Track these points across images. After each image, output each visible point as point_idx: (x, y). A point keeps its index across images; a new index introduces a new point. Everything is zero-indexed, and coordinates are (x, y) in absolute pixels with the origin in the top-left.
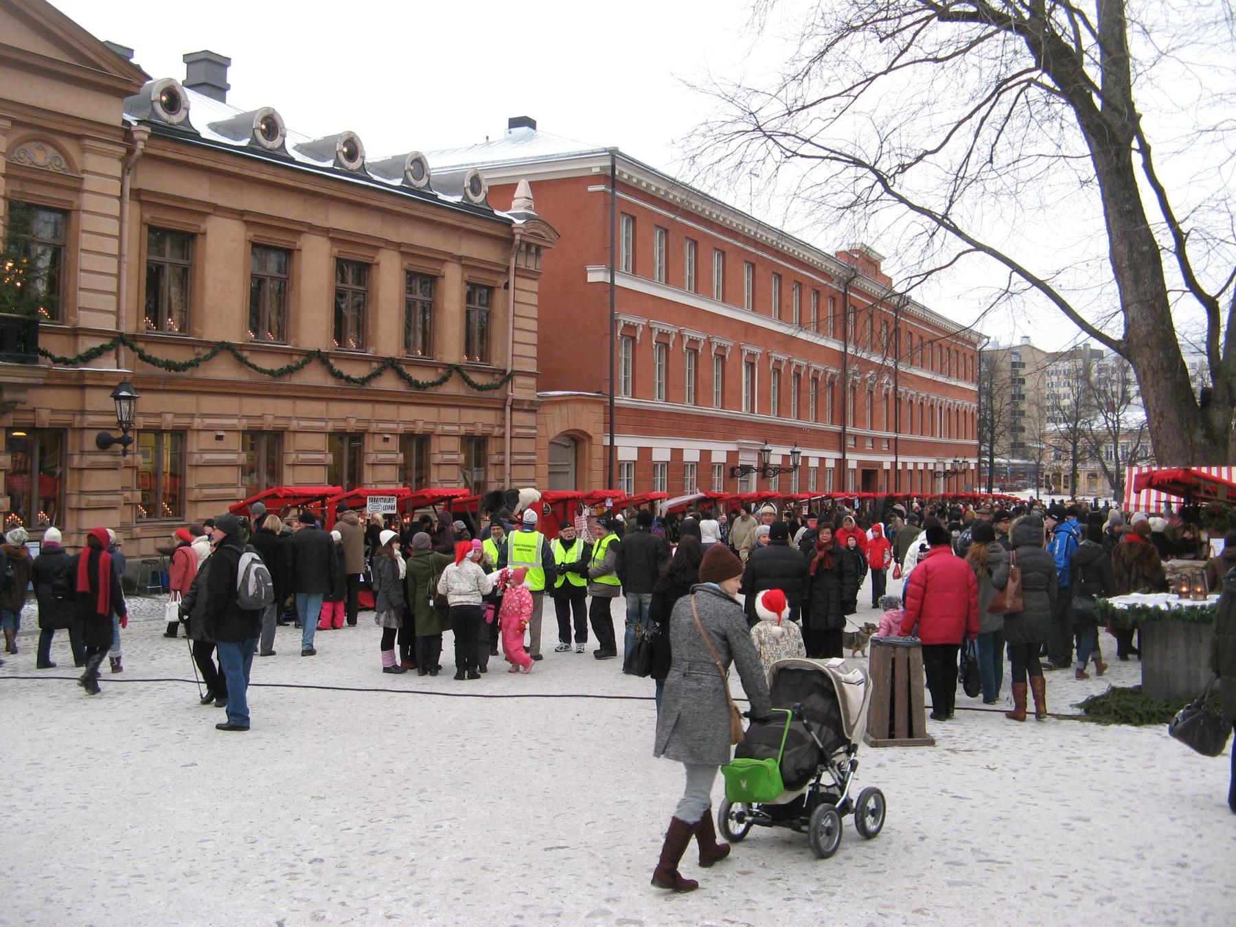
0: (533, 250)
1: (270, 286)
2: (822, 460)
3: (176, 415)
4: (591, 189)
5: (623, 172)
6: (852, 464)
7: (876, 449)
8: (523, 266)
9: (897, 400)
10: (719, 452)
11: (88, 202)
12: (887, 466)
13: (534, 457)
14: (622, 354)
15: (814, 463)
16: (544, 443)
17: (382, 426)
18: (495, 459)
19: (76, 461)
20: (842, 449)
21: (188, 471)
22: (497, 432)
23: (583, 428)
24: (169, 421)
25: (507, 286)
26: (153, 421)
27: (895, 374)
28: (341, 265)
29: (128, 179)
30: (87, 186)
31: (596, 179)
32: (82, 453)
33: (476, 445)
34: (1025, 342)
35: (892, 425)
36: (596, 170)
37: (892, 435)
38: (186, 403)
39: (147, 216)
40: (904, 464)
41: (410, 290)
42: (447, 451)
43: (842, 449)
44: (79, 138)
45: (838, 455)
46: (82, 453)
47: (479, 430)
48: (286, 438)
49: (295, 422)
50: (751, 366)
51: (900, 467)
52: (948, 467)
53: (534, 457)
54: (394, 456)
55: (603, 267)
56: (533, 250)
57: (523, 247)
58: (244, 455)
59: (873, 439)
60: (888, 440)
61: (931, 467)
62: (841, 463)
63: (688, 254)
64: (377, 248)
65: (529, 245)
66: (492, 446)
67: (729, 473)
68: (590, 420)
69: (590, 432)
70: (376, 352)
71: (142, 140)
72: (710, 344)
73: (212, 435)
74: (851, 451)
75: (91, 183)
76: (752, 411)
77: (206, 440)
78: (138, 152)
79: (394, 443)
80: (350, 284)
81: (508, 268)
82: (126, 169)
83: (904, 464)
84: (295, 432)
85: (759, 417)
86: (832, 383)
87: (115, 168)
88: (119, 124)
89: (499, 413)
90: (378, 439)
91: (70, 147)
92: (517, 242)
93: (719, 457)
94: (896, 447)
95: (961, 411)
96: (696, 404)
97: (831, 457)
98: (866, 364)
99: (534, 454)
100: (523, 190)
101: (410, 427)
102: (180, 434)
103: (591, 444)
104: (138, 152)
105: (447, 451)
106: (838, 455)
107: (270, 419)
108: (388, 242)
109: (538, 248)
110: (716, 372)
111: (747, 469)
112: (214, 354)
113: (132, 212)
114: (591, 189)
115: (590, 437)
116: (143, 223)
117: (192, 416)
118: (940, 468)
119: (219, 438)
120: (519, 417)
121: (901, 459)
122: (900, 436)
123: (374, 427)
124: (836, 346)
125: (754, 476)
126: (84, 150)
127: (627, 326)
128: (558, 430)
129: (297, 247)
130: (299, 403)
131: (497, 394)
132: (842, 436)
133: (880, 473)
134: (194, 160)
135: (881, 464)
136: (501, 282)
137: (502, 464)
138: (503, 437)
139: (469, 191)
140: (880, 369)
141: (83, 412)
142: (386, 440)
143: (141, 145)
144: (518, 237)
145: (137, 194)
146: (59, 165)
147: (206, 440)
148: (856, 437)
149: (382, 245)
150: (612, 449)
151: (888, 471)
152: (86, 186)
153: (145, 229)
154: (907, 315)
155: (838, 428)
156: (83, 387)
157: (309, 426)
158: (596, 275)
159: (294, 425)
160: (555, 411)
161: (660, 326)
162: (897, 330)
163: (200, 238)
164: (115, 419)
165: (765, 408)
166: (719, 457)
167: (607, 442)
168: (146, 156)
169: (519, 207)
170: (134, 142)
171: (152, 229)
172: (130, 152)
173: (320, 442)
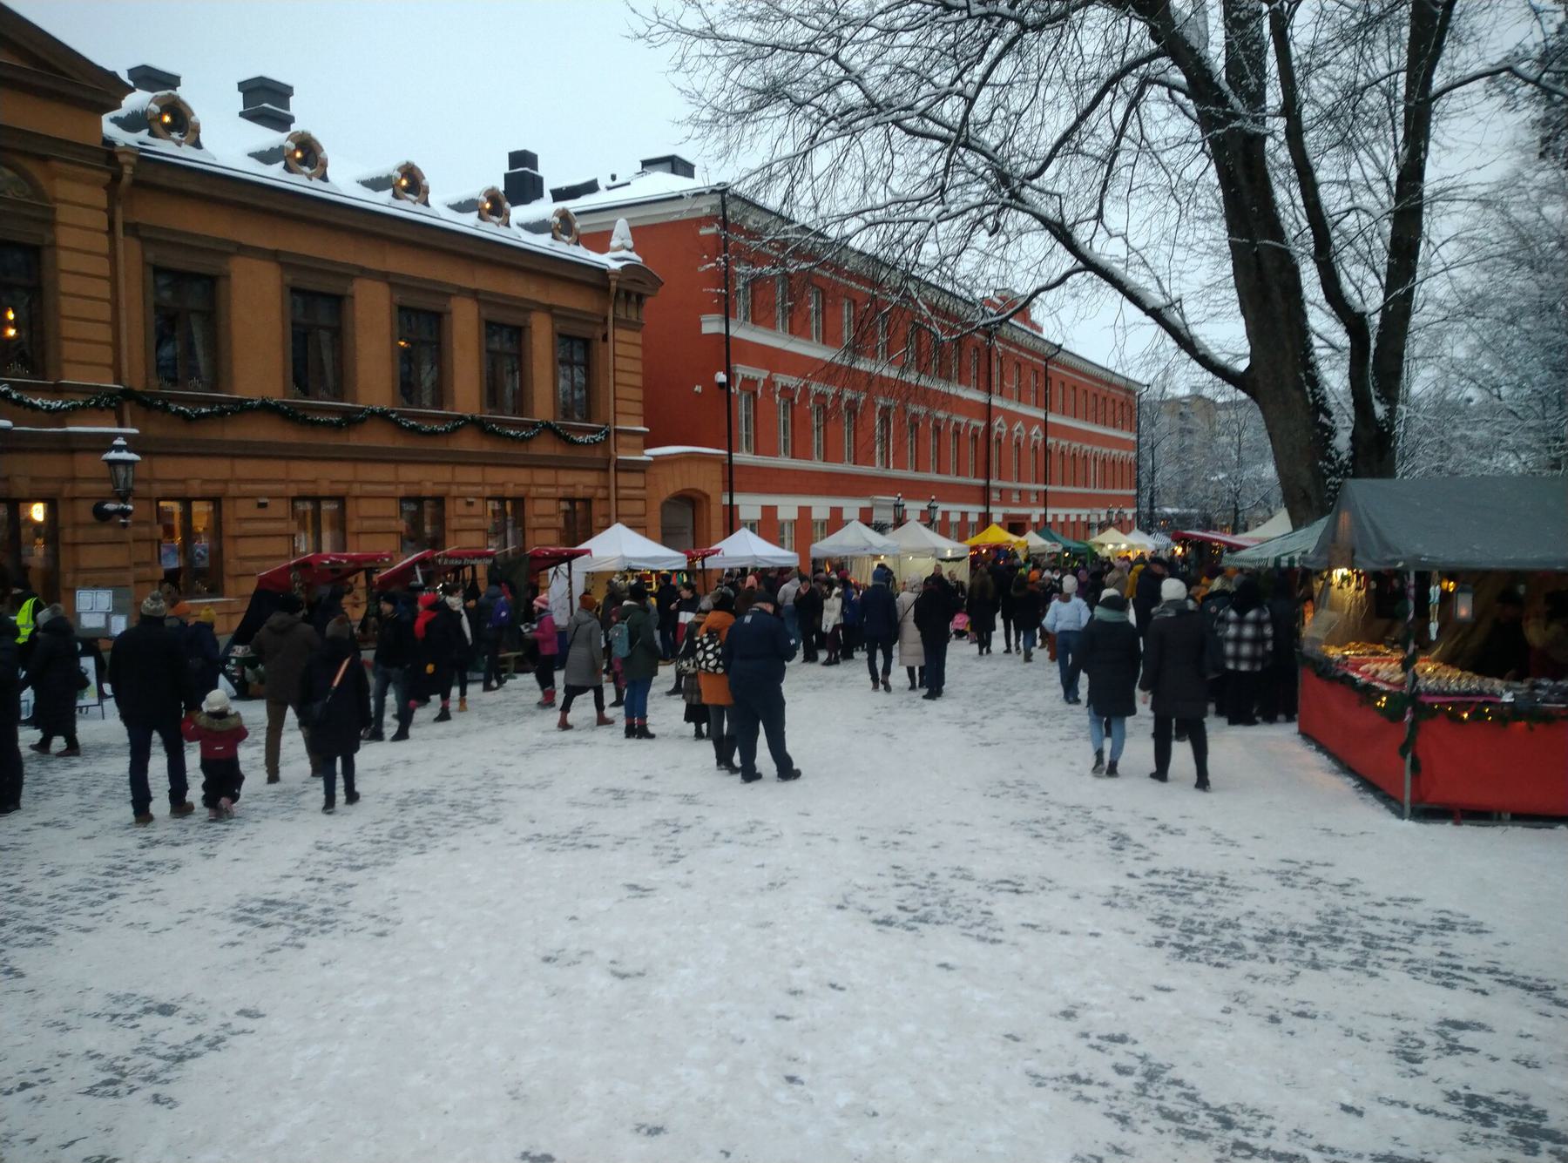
0: (634, 298)
3: (205, 481)
7: (1024, 501)
8: (623, 316)
9: (1047, 451)
11: (65, 237)
16: (657, 506)
17: (463, 489)
20: (987, 502)
22: (601, 493)
23: (700, 487)
24: (510, 491)
25: (605, 338)
26: (499, 491)
27: (1045, 425)
29: (119, 211)
30: (61, 218)
31: (708, 220)
32: (76, 525)
36: (707, 211)
37: (1041, 487)
38: (443, 473)
39: (150, 256)
40: (1055, 516)
43: (987, 502)
44: (43, 159)
45: (982, 509)
46: (76, 525)
47: (581, 492)
50: (885, 420)
51: (1049, 519)
52: (1103, 518)
54: (393, 523)
55: (717, 316)
56: (634, 298)
57: (622, 295)
59: (1020, 492)
60: (1037, 493)
61: (1084, 518)
64: (529, 311)
65: (628, 294)
69: (707, 490)
71: (128, 163)
72: (841, 397)
73: (251, 504)
74: (996, 504)
75: (64, 214)
77: (460, 503)
81: (606, 319)
82: (112, 186)
83: (1055, 516)
84: (235, 498)
86: (975, 436)
87: (101, 199)
88: (98, 144)
90: (460, 503)
91: (31, 166)
92: (613, 290)
94: (1045, 499)
98: (1011, 417)
100: (621, 231)
101: (570, 490)
102: (439, 501)
103: (709, 505)
104: (126, 180)
106: (982, 509)
109: (640, 297)
110: (932, 442)
112: (455, 429)
113: (130, 253)
115: (707, 497)
116: (145, 264)
118: (1094, 519)
119: (263, 506)
120: (623, 479)
121: (1051, 511)
122: (1050, 488)
123: (454, 490)
124: (980, 397)
127: (746, 380)
128: (671, 492)
131: (599, 454)
132: (986, 490)
135: (1028, 517)
136: (599, 333)
138: (607, 499)
140: (1029, 421)
142: (470, 504)
144: (613, 284)
145: (132, 229)
148: (1001, 491)
154: (1059, 364)
155: (982, 482)
156: (73, 451)
157: (471, 492)
158: (711, 325)
159: (357, 489)
161: (782, 380)
162: (1048, 379)
164: (110, 486)
165: (900, 465)
167: (726, 500)
170: (120, 166)
172: (116, 178)
173: (391, 507)
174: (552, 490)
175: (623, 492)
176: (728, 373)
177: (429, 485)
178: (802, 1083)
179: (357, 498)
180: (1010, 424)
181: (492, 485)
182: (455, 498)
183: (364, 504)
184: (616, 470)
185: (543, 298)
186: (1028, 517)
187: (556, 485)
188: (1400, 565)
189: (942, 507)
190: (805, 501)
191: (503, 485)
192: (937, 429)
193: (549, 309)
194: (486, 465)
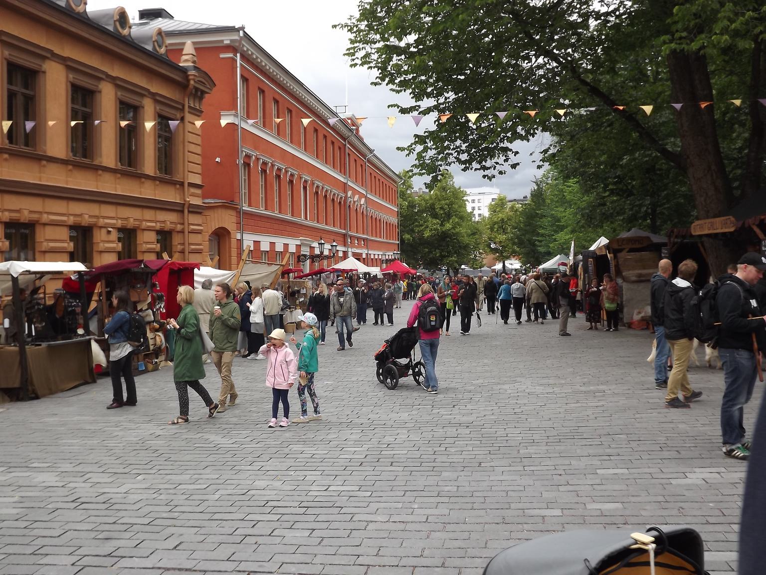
3: (31, 212)
4: (222, 56)
7: (359, 246)
8: (192, 105)
10: (293, 244)
13: (201, 247)
14: (242, 175)
22: (179, 227)
33: (165, 236)
35: (343, 226)
36: (227, 42)
47: (168, 226)
48: (173, 236)
49: (45, 216)
50: (305, 188)
52: (317, 252)
53: (201, 247)
54: (65, 245)
58: (120, 244)
64: (100, 79)
66: (176, 240)
67: (296, 260)
68: (227, 220)
70: (101, 163)
72: (301, 178)
76: (306, 218)
79: (114, 235)
81: (183, 106)
89: (179, 214)
90: (104, 231)
93: (292, 249)
95: (378, 218)
96: (280, 212)
98: (355, 192)
99: (200, 244)
101: (78, 219)
103: (230, 238)
107: (26, 213)
109: (203, 93)
114: (222, 56)
115: (228, 233)
118: (305, 251)
123: (102, 222)
129: (43, 70)
130: (158, 212)
138: (182, 232)
142: (109, 232)
144: (192, 82)
149: (104, 77)
150: (240, 242)
151: (364, 259)
159: (45, 218)
163: (41, 74)
169: (186, 61)
173: (64, 233)
174: (154, 224)
175: (192, 227)
177: (26, 213)
178: (506, 323)
179: (45, 224)
180: (360, 198)
181: (75, 215)
182: (101, 227)
183: (48, 229)
184: (189, 212)
185: (154, 89)
187: (156, 222)
188: (762, 185)
190: (273, 240)
191: (18, 211)
192: (264, 171)
193: (113, 80)
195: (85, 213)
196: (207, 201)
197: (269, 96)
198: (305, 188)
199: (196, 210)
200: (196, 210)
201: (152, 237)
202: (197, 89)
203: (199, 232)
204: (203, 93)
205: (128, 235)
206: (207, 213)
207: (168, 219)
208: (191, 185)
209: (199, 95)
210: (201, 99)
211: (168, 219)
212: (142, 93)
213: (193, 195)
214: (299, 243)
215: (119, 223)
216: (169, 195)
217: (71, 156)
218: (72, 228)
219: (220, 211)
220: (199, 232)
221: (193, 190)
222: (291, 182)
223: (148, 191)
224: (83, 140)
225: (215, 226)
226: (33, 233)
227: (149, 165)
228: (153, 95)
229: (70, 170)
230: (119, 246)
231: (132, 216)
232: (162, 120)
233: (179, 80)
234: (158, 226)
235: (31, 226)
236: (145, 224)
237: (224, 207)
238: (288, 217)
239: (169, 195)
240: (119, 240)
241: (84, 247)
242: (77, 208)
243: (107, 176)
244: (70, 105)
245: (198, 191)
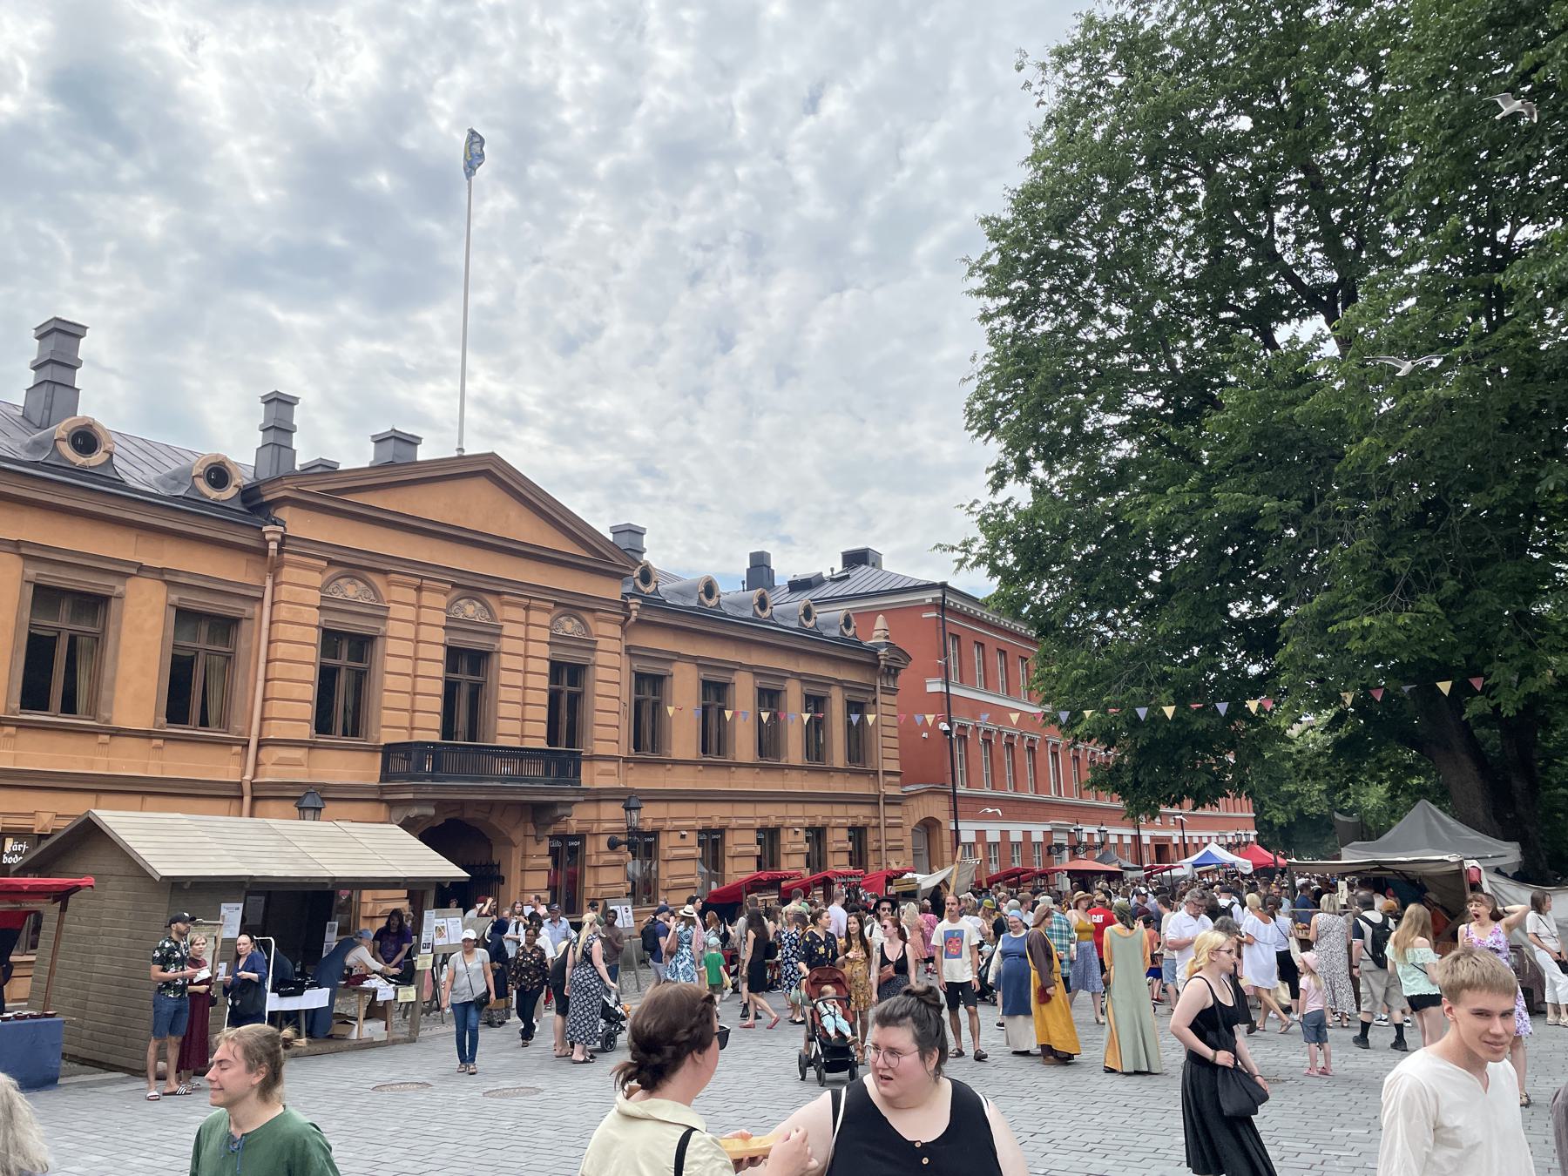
1: (343, 680)
2: (1120, 836)
5: (951, 600)
6: (1146, 840)
10: (1038, 832)
12: (1176, 840)
15: (1113, 840)
18: (875, 845)
19: (593, 861)
21: (783, 858)
22: (874, 822)
25: (875, 701)
28: (706, 685)
32: (598, 853)
34: (624, 542)
41: (638, 690)
42: (838, 839)
46: (598, 853)
47: (861, 822)
50: (1055, 754)
62: (1137, 839)
63: (999, 662)
66: (871, 836)
68: (937, 808)
73: (677, 835)
74: (1146, 828)
78: (633, 619)
79: (802, 835)
80: (343, 661)
85: (1065, 799)
90: (791, 832)
91: (376, 579)
93: (1038, 837)
97: (1128, 833)
101: (707, 822)
104: (633, 619)
105: (838, 839)
106: (1134, 832)
108: (141, 568)
109: (897, 669)
110: (1007, 759)
111: (1060, 847)
115: (939, 823)
117: (664, 819)
123: (788, 823)
125: (1066, 853)
126: (390, 584)
130: (701, 805)
133: (1171, 848)
134: (57, 500)
135: (1170, 839)
136: (870, 699)
137: (879, 850)
139: (638, 582)
141: (599, 821)
142: (683, 836)
143: (634, 614)
146: (366, 598)
147: (674, 839)
152: (391, 614)
153: (173, 612)
159: (734, 823)
160: (914, 802)
163: (245, 625)
164: (624, 825)
166: (1038, 837)
168: (640, 622)
171: (637, 674)
172: (627, 618)
173: (751, 837)
176: (950, 724)
186: (1170, 839)
187: (847, 817)
189: (1087, 829)
190: (1005, 827)
192: (987, 742)
193: (797, 676)
194: (599, 801)
195: (715, 814)
196: (908, 788)
197: (991, 648)
198: (1055, 754)
199: (893, 801)
200: (893, 801)
201: (843, 834)
202: (889, 667)
203: (899, 826)
204: (897, 669)
205: (769, 836)
206: (909, 802)
207: (861, 814)
208: (886, 773)
209: (892, 672)
210: (895, 676)
211: (861, 814)
212: (782, 676)
213: (890, 784)
214: (1048, 828)
215: (807, 823)
216: (861, 787)
217: (806, 763)
218: (850, 829)
219: (926, 799)
220: (899, 826)
221: (889, 779)
222: (1031, 749)
223: (838, 786)
224: (769, 741)
225: (919, 816)
226: (657, 842)
227: (838, 757)
228: (840, 683)
229: (158, 748)
230: (807, 847)
231: (771, 814)
232: (855, 707)
233: (867, 659)
234: (850, 822)
235: (721, 831)
236: (834, 822)
237: (931, 792)
238: (1029, 795)
239: (861, 787)
240: (807, 839)
241: (772, 848)
242: (854, 810)
243: (794, 774)
244: (26, 616)
245: (897, 779)
